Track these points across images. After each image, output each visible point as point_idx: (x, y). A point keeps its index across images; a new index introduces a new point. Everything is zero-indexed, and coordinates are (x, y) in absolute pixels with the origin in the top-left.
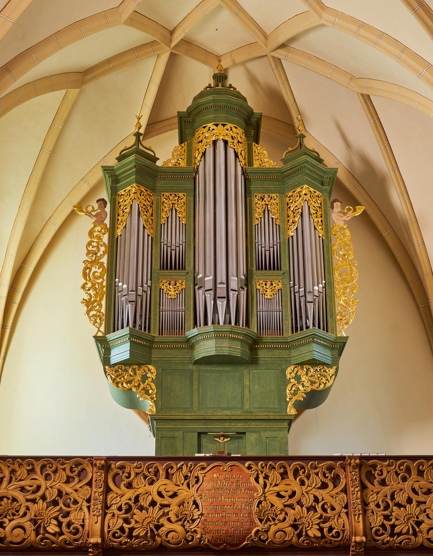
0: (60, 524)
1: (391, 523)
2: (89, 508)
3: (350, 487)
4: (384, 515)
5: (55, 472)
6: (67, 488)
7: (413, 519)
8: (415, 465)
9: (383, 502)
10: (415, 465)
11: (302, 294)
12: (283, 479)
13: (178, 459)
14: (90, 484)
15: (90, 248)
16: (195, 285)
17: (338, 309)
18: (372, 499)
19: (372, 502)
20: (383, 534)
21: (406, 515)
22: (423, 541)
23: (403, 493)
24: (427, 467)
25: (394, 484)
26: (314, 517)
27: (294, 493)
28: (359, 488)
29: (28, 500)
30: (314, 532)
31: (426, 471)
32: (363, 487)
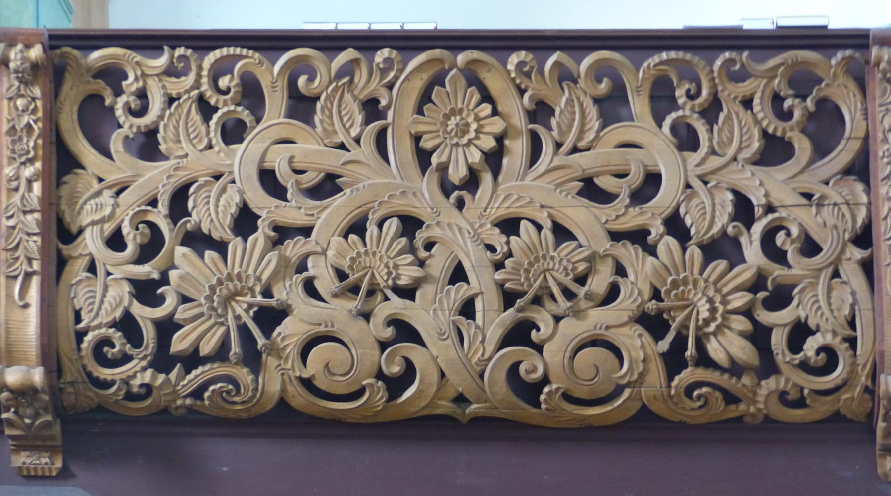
1: (159, 313)
3: (5, 161)
4: (133, 282)
7: (248, 298)
8: (277, 68)
9: (137, 229)
10: (277, 68)
12: (607, 119)
18: (95, 211)
19: (93, 223)
20: (126, 359)
21: (220, 282)
22: (283, 390)
23: (223, 190)
24: (326, 80)
25: (191, 149)
28: (38, 165)
31: (323, 98)
32: (64, 163)
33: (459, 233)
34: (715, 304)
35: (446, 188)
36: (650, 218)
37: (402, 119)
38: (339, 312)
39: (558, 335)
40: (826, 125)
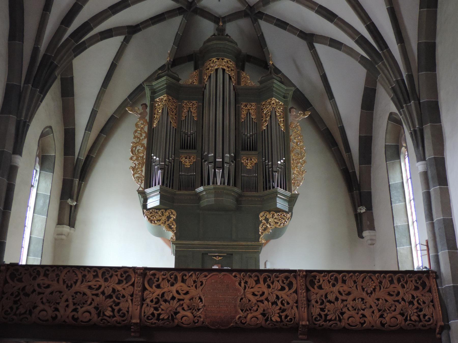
0: (113, 310)
2: (132, 300)
5: (111, 277)
6: (119, 287)
11: (270, 166)
13: (189, 270)
14: (133, 285)
15: (136, 134)
16: (202, 159)
17: (293, 176)
18: (313, 297)
25: (327, 287)
26: (276, 309)
27: (263, 293)
29: (93, 295)
30: (275, 318)
32: (308, 290)
33: (370, 300)
34: (411, 311)
35: (368, 294)
36: (399, 298)
37: (359, 283)
38: (353, 313)
39: (388, 317)
40: (424, 285)
